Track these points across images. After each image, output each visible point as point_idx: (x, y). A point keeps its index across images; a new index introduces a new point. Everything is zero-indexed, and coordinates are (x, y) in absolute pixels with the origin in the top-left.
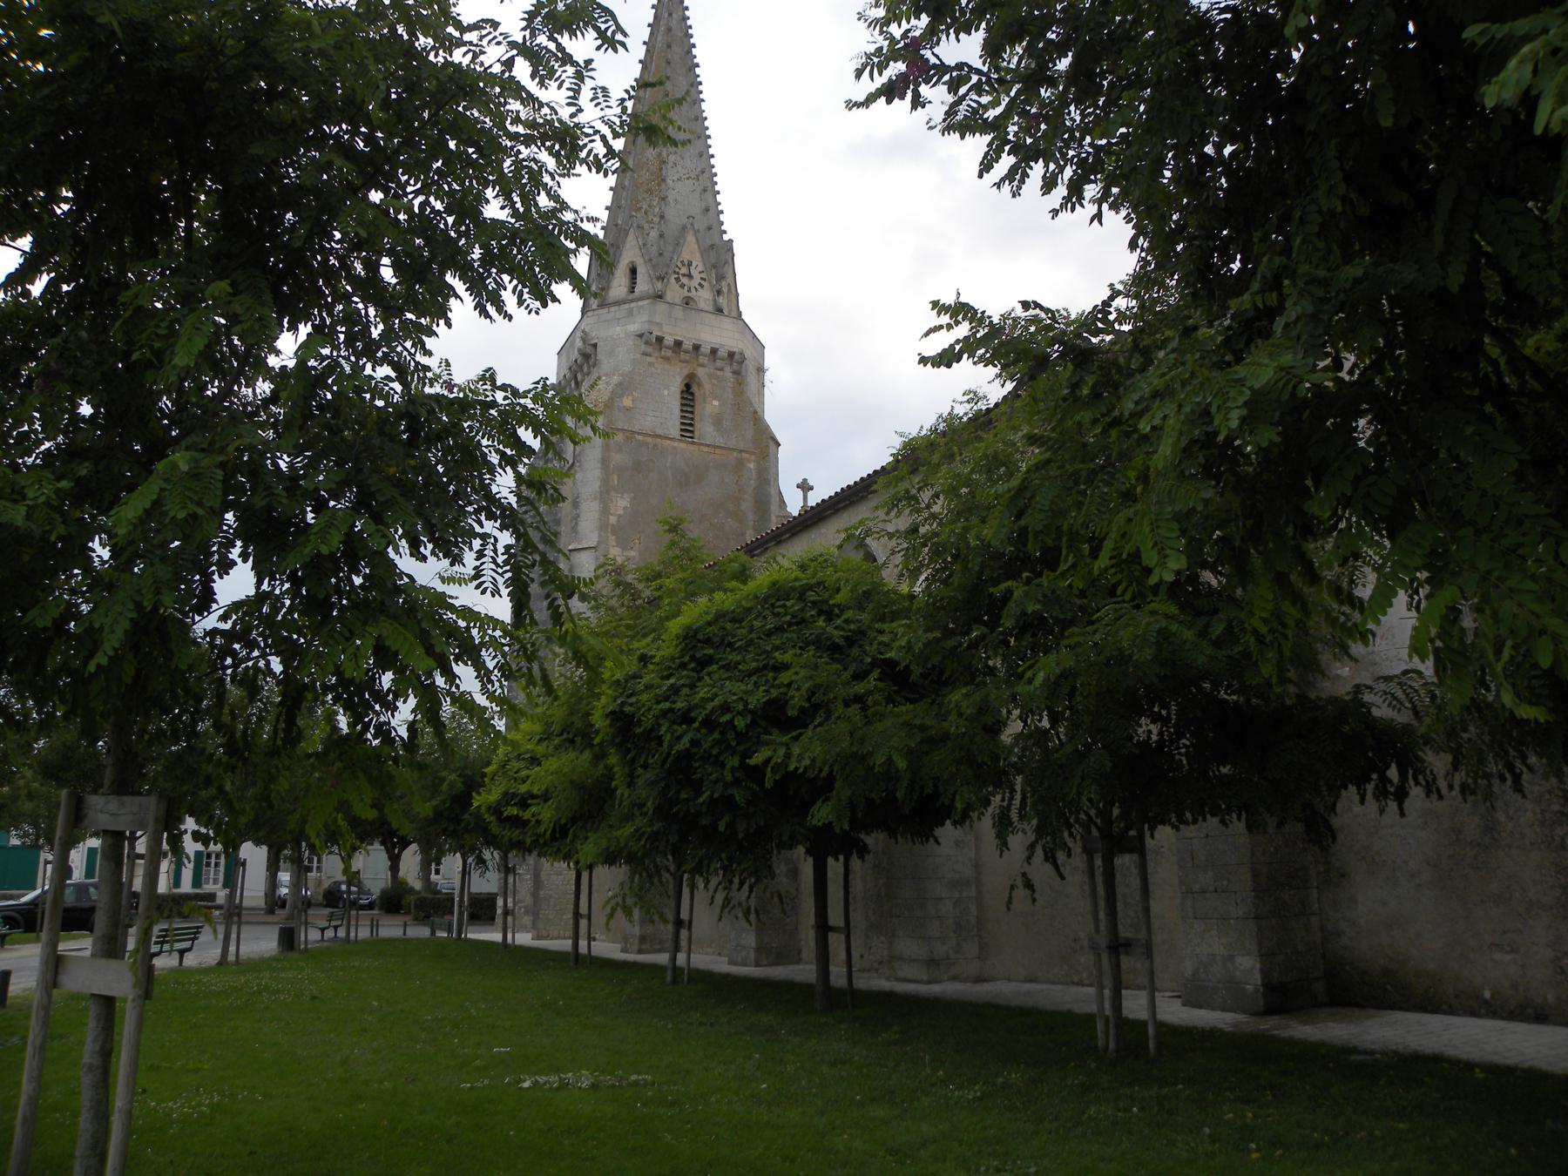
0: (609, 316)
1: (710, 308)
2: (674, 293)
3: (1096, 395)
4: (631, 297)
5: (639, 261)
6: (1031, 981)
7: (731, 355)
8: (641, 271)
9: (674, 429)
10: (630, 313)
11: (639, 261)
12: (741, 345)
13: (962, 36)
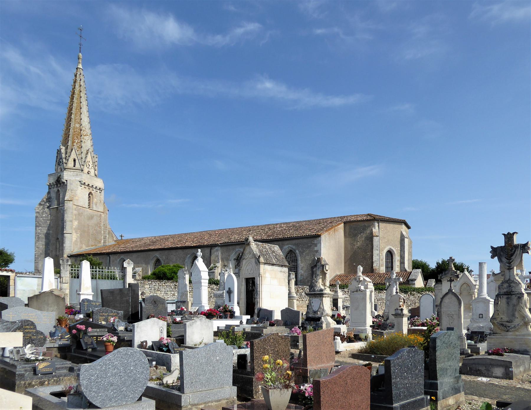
2: (86, 170)
4: (74, 168)
8: (77, 161)
9: (87, 206)
11: (76, 159)
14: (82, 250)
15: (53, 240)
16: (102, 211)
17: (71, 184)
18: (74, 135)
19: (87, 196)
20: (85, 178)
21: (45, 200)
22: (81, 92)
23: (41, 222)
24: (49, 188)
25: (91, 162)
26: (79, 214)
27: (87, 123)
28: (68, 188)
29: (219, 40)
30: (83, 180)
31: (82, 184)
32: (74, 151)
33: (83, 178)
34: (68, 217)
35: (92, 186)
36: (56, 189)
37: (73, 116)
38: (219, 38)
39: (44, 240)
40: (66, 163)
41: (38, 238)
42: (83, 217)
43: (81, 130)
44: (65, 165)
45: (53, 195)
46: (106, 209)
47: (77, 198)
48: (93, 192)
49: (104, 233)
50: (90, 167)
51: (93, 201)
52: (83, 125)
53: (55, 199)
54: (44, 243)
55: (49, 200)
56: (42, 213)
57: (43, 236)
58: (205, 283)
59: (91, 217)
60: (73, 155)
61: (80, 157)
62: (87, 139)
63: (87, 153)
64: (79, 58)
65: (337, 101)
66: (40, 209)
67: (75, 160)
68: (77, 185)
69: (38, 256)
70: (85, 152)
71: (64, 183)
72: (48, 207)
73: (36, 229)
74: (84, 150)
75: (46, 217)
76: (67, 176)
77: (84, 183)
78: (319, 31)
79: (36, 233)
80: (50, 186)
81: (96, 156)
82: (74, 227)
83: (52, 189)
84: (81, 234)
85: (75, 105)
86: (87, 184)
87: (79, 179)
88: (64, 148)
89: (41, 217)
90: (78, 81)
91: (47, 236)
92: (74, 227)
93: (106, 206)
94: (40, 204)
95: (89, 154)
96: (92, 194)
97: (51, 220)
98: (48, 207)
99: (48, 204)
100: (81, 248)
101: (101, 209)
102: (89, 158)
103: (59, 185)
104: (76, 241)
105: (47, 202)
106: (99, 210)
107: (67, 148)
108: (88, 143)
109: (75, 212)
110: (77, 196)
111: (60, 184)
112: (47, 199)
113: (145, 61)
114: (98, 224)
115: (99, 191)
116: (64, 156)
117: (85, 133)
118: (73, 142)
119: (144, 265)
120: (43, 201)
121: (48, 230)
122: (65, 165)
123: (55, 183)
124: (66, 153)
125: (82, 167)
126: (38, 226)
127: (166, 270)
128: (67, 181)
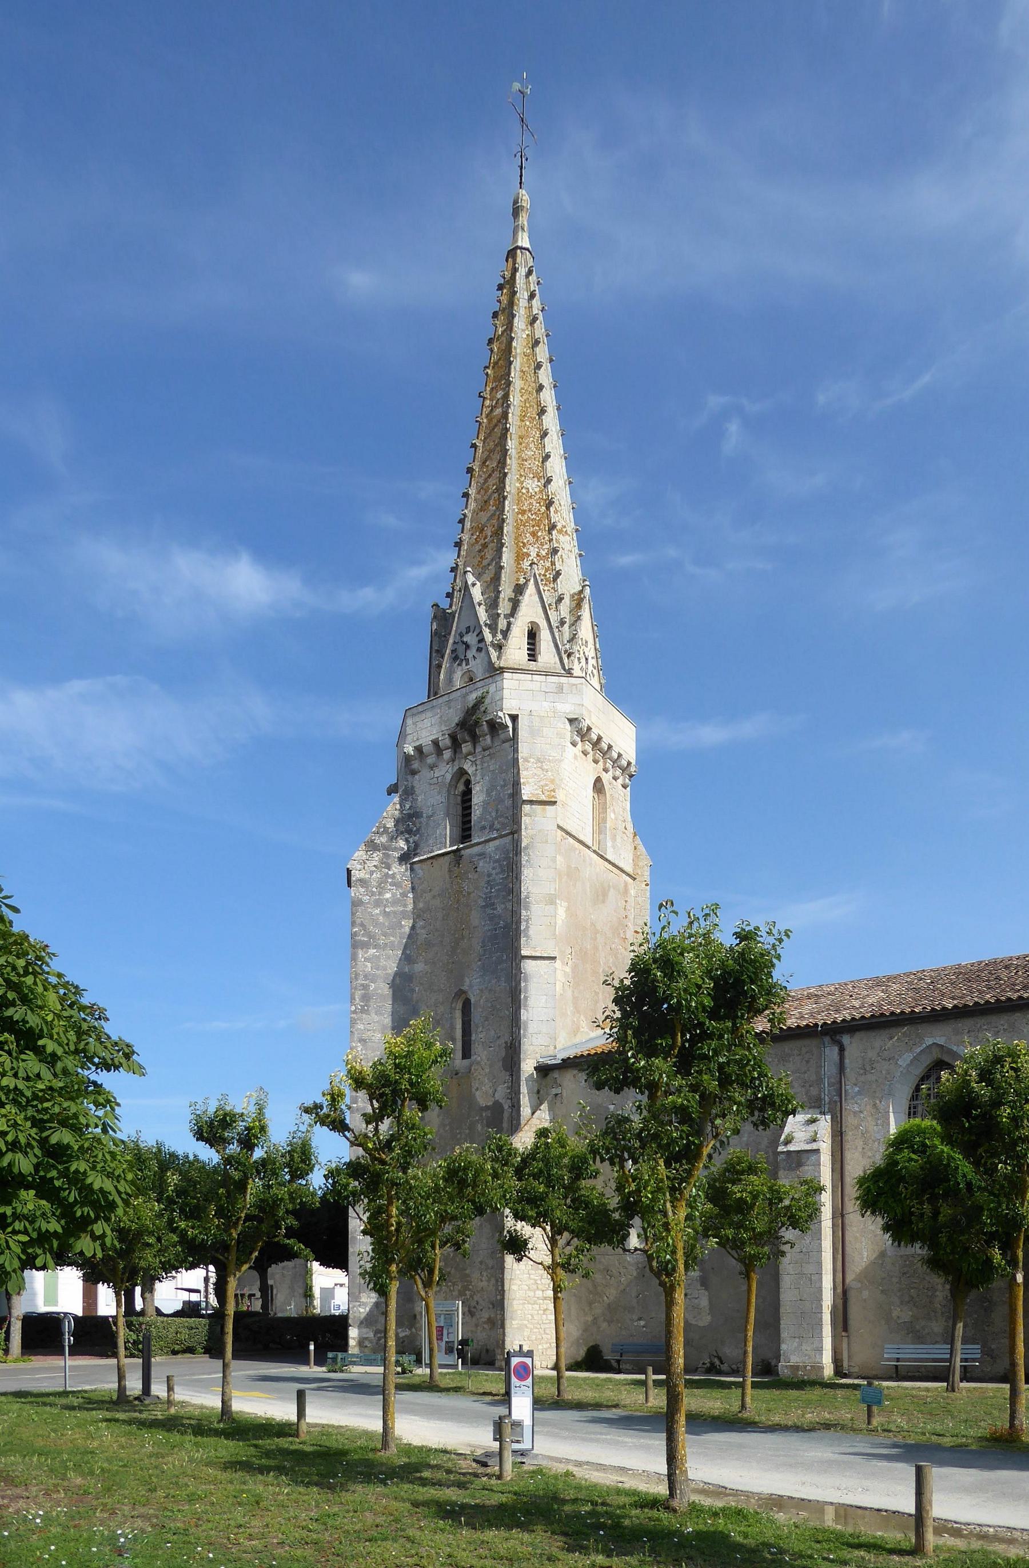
0: (535, 686)
8: (545, 636)
14: (577, 1040)
17: (533, 733)
18: (519, 525)
21: (390, 824)
23: (377, 924)
27: (561, 482)
32: (531, 589)
34: (537, 879)
36: (445, 772)
38: (367, 594)
39: (388, 1006)
40: (499, 647)
44: (494, 654)
53: (440, 814)
54: (388, 1021)
55: (409, 823)
57: (386, 990)
58: (51, 1295)
60: (530, 610)
64: (516, 211)
65: (711, 734)
66: (370, 864)
67: (532, 635)
71: (495, 727)
72: (404, 858)
75: (395, 902)
76: (517, 696)
78: (626, 560)
83: (425, 774)
84: (575, 968)
85: (515, 399)
87: (567, 707)
89: (378, 903)
91: (402, 987)
93: (642, 848)
95: (586, 606)
97: (417, 915)
98: (404, 858)
99: (402, 844)
103: (466, 748)
107: (493, 585)
111: (475, 739)
112: (397, 822)
113: (180, 666)
116: (482, 614)
121: (407, 958)
122: (494, 654)
124: (493, 605)
126: (365, 946)
128: (514, 718)
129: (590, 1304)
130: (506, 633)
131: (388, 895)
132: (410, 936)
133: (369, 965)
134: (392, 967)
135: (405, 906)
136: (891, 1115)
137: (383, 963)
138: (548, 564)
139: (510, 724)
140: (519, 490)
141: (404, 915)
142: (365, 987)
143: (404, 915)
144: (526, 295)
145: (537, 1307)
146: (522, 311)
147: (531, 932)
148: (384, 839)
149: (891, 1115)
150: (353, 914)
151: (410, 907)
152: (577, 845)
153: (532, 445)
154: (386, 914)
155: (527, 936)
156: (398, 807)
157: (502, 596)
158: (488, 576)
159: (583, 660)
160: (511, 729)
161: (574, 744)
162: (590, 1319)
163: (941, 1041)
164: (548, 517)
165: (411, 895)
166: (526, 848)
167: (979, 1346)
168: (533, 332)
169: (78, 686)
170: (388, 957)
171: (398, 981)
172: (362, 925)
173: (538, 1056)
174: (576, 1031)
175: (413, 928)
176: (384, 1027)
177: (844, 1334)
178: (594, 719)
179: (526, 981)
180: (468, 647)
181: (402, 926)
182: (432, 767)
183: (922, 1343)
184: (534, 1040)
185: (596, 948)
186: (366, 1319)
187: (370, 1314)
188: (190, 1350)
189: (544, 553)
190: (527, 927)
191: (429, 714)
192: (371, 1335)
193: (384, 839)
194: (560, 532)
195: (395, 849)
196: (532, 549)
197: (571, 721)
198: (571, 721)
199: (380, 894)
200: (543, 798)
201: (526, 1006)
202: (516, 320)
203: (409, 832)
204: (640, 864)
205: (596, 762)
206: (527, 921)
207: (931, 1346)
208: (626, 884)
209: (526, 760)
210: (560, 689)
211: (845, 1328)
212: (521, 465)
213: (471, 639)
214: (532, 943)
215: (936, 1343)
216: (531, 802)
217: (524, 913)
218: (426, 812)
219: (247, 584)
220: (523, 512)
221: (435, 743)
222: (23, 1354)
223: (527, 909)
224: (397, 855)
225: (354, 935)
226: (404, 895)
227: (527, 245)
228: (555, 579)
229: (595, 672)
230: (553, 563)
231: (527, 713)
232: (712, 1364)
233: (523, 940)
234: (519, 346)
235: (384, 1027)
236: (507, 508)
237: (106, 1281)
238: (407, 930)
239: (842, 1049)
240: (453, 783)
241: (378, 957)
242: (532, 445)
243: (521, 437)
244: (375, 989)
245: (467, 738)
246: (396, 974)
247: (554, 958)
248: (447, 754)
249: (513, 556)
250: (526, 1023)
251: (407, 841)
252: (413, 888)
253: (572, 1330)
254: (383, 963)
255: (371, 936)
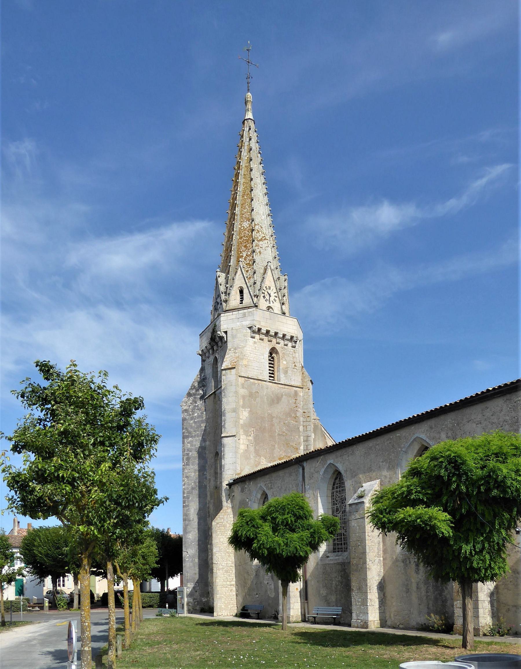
0: (234, 317)
1: (280, 313)
2: (263, 304)
3: (144, 476)
4: (241, 306)
5: (244, 286)
6: (394, 628)
7: (292, 337)
8: (246, 291)
9: (266, 377)
10: (244, 315)
11: (244, 286)
12: (296, 333)
13: (160, 496)
15: (210, 456)
16: (299, 384)
17: (234, 337)
18: (239, 244)
19: (267, 354)
20: (260, 318)
21: (196, 384)
22: (251, 160)
24: (203, 361)
25: (273, 287)
26: (251, 395)
27: (263, 217)
28: (229, 345)
29: (453, 204)
30: (255, 323)
31: (254, 332)
32: (239, 272)
33: (257, 318)
34: (229, 402)
35: (276, 334)
36: (212, 359)
37: (237, 210)
39: (197, 461)
40: (226, 301)
41: (187, 460)
42: (258, 399)
43: (253, 230)
45: (209, 371)
46: (308, 379)
47: (245, 362)
48: (278, 347)
49: (306, 430)
50: (272, 299)
51: (279, 366)
52: (256, 221)
53: (211, 376)
54: (196, 467)
56: (193, 409)
57: (196, 454)
59: (276, 400)
60: (239, 282)
61: (251, 282)
62: (264, 246)
63: (265, 273)
64: (246, 103)
67: (241, 292)
68: (245, 336)
69: (188, 493)
70: (262, 271)
71: (221, 338)
72: (202, 398)
73: (183, 443)
74: (259, 267)
75: (199, 417)
76: (227, 323)
77: (259, 330)
79: (184, 451)
80: (203, 354)
81: (283, 278)
82: (241, 422)
83: (207, 360)
84: (256, 438)
85: (241, 188)
86: (264, 331)
88: (223, 275)
89: (192, 419)
90: (247, 144)
92: (241, 422)
93: (306, 373)
94: (189, 395)
95: (269, 272)
96: (277, 353)
97: (207, 421)
98: (202, 398)
99: (201, 392)
100: (257, 466)
101: (296, 380)
102: (269, 281)
103: (215, 348)
104: (246, 451)
105: (200, 387)
106: (293, 383)
108: (266, 253)
109: (242, 392)
110: (247, 356)
111: (217, 344)
112: (199, 383)
114: (292, 413)
115: (290, 344)
116: (222, 289)
117: (260, 236)
118: (239, 257)
119: (385, 473)
120: (193, 387)
121: (204, 440)
123: (209, 347)
125: (255, 299)
126: (187, 437)
127: (463, 451)
129: (244, 587)
130: (229, 294)
131: (196, 414)
132: (205, 430)
133: (189, 445)
134: (198, 445)
135: (203, 418)
136: (319, 498)
137: (194, 443)
138: (251, 258)
139: (224, 335)
140: (240, 228)
141: (202, 422)
142: (188, 454)
143: (202, 422)
144: (248, 139)
145: (227, 589)
146: (246, 148)
147: (226, 426)
148: (194, 391)
149: (319, 498)
150: (183, 424)
151: (204, 418)
152: (256, 381)
153: (247, 207)
154: (195, 422)
155: (225, 428)
156: (199, 376)
157: (230, 278)
158: (227, 271)
159: (267, 297)
160: (225, 338)
161: (253, 338)
162: (244, 594)
163: (332, 461)
164: (252, 236)
165: (204, 413)
166: (224, 389)
167: (341, 608)
168: (250, 155)
169: (308, 289)
170: (196, 440)
171: (200, 450)
172: (186, 429)
173: (229, 479)
174: (259, 463)
175: (206, 427)
176: (195, 470)
177: (305, 601)
178: (263, 324)
179: (224, 447)
180: (218, 303)
181: (201, 427)
182: (208, 357)
183: (330, 606)
184: (227, 472)
185: (273, 425)
186: (190, 594)
187: (191, 592)
188: (151, 606)
189: (249, 253)
190: (225, 424)
191: (204, 336)
192: (192, 601)
193: (194, 391)
194: (261, 240)
195: (198, 395)
196: (244, 253)
197: (250, 328)
198: (250, 328)
199: (193, 414)
200: (230, 367)
201: (224, 458)
202: (242, 153)
203: (204, 386)
204: (305, 380)
205: (270, 341)
206: (224, 421)
207: (332, 608)
208: (296, 392)
209: (230, 350)
210: (244, 315)
211: (306, 599)
212: (241, 217)
213: (218, 300)
214: (227, 430)
215: (333, 606)
216: (225, 369)
217: (223, 418)
218: (208, 377)
219: (388, 216)
220: (241, 238)
221: (206, 347)
222: (108, 607)
223: (224, 416)
224: (199, 397)
225: (183, 433)
226: (202, 413)
227: (252, 118)
228: (253, 264)
229: (277, 299)
230: (253, 257)
231: (230, 329)
232: (275, 615)
233: (223, 429)
234: (243, 164)
235: (195, 470)
236: (234, 238)
237: (474, 567)
238: (203, 428)
239: (303, 469)
240: (215, 362)
241: (192, 441)
242: (247, 207)
243: (242, 205)
244: (192, 455)
245: (214, 344)
246: (200, 447)
247: (234, 436)
248: (211, 351)
249: (236, 259)
250: (224, 465)
251: (203, 390)
252: (205, 410)
253: (240, 599)
254: (194, 443)
255: (190, 433)
